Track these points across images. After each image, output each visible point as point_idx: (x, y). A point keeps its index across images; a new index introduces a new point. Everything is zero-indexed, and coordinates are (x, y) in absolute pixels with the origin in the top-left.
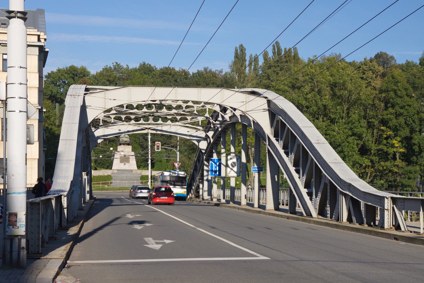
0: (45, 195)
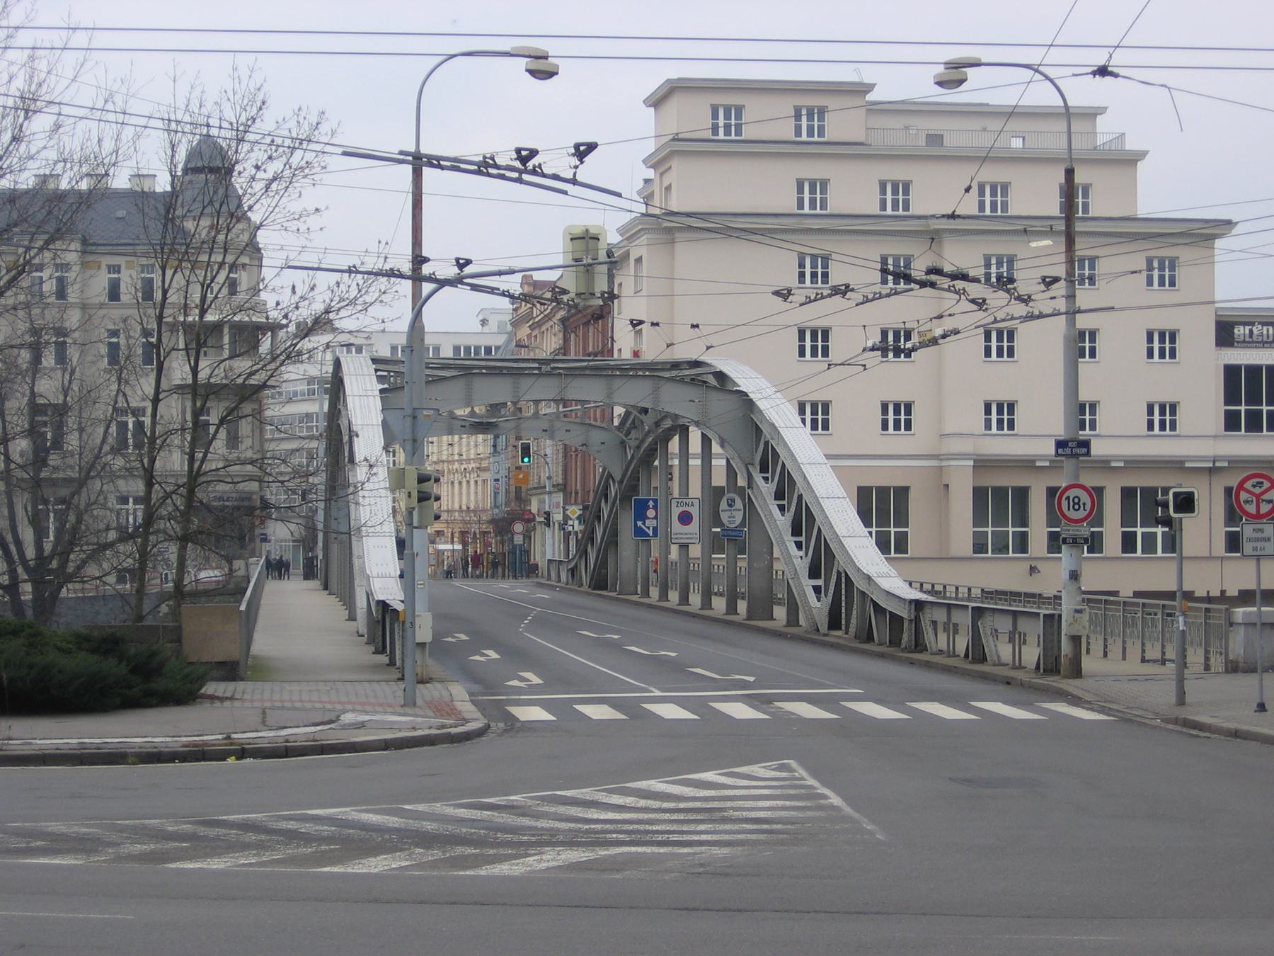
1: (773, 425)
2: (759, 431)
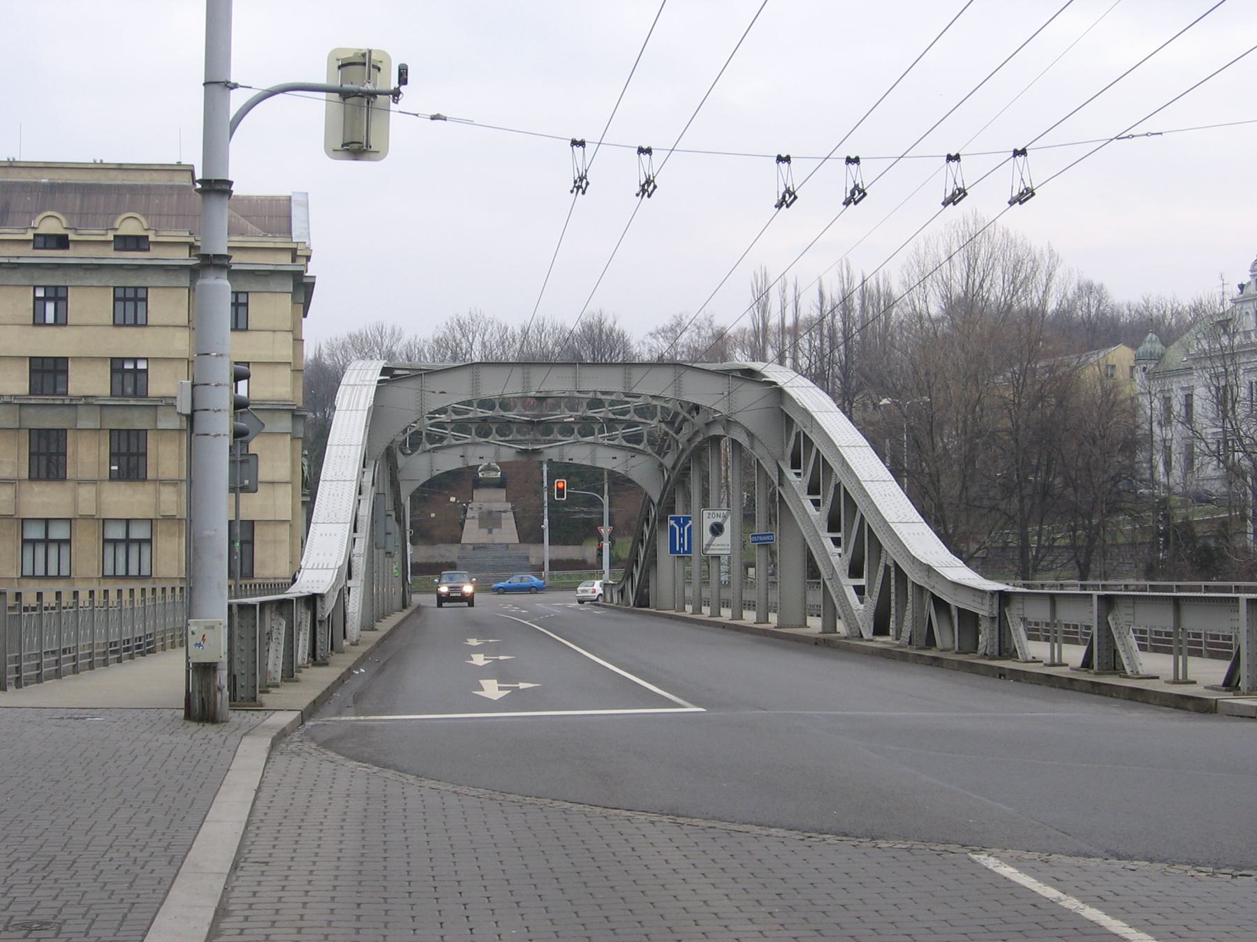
0: (283, 593)
1: (805, 410)
2: (789, 421)
